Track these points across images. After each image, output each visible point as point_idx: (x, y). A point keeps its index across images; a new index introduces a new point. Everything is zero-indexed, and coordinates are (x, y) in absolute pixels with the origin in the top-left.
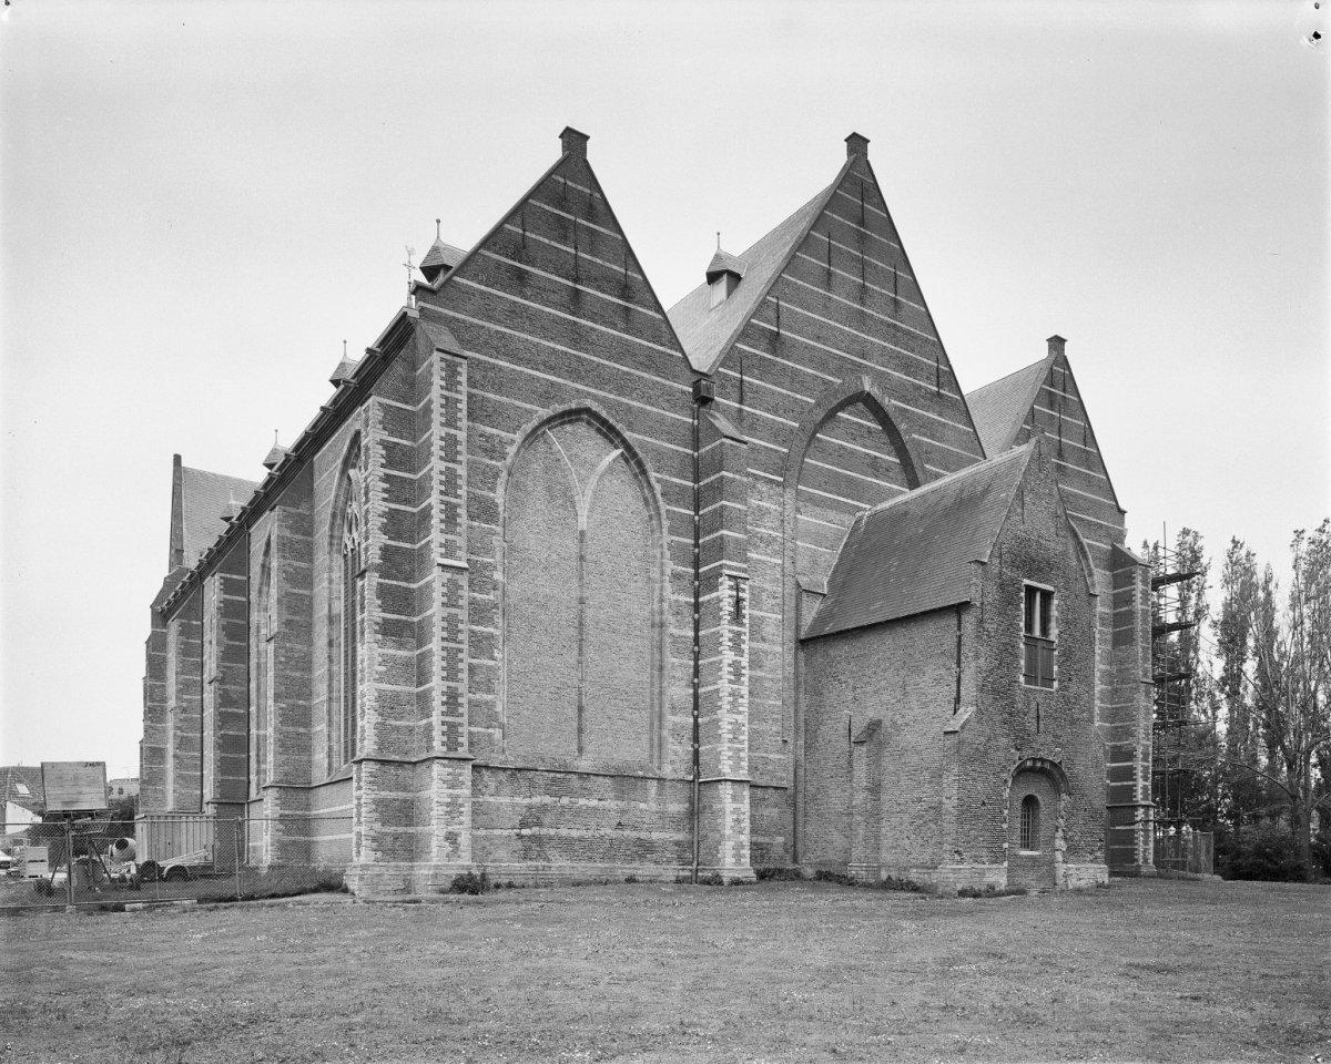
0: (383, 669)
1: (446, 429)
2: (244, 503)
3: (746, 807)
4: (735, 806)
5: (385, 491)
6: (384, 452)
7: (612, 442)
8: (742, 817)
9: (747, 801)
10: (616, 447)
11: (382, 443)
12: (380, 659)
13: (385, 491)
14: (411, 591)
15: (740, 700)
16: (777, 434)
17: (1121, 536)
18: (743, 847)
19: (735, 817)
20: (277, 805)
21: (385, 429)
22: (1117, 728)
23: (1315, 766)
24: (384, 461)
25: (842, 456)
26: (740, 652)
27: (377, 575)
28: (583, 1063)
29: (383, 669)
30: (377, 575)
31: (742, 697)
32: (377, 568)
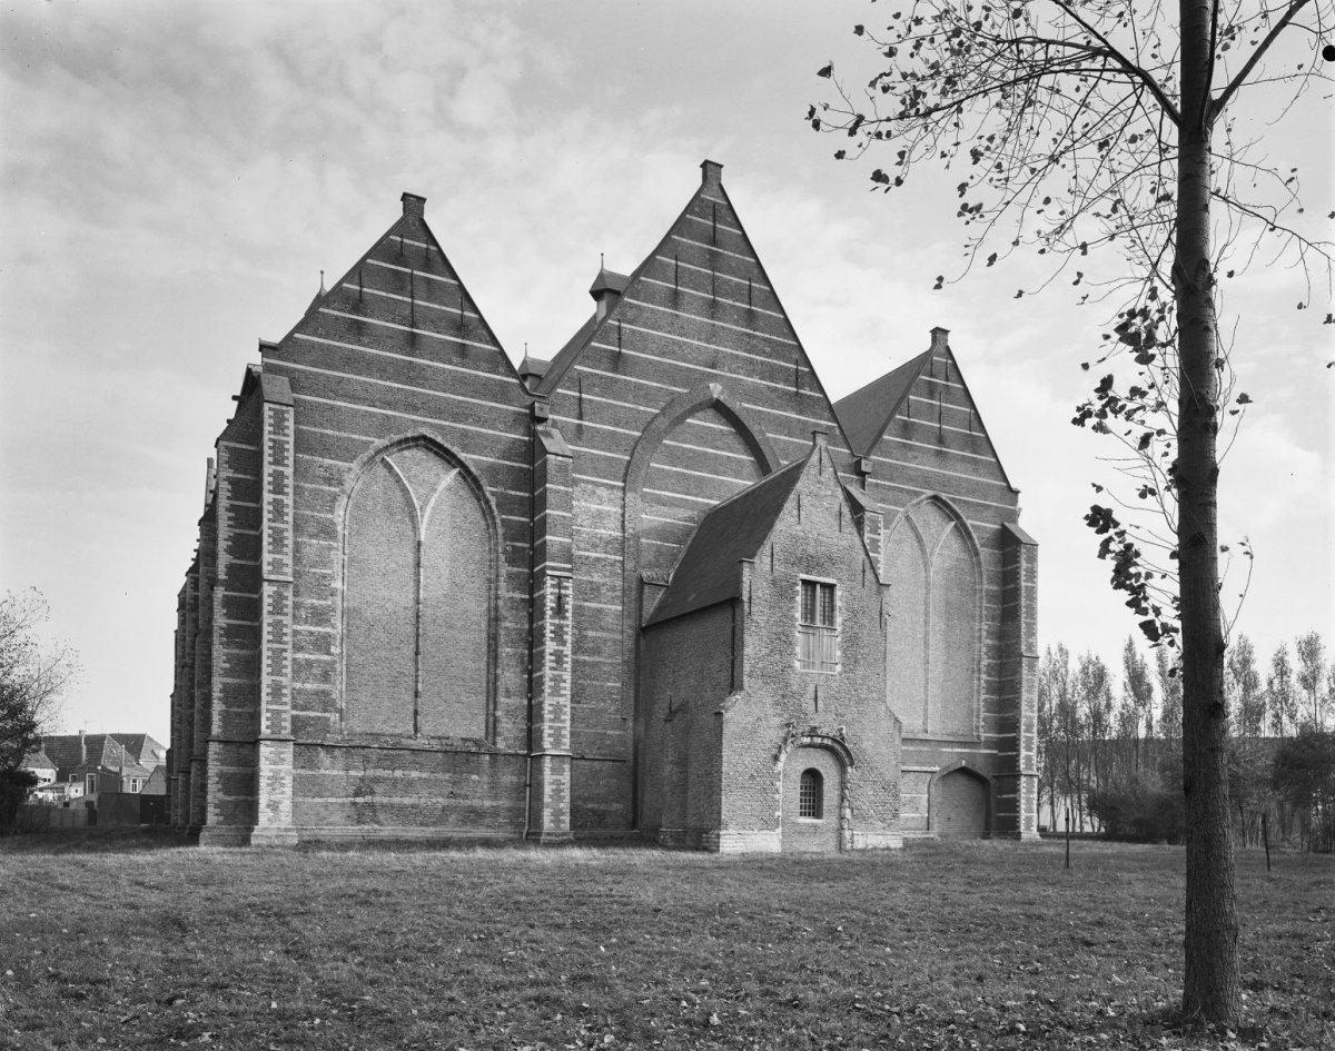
0: (228, 665)
5: (230, 518)
15: (562, 685)
16: (612, 441)
17: (1013, 516)
19: (554, 787)
27: (223, 589)
32: (224, 583)
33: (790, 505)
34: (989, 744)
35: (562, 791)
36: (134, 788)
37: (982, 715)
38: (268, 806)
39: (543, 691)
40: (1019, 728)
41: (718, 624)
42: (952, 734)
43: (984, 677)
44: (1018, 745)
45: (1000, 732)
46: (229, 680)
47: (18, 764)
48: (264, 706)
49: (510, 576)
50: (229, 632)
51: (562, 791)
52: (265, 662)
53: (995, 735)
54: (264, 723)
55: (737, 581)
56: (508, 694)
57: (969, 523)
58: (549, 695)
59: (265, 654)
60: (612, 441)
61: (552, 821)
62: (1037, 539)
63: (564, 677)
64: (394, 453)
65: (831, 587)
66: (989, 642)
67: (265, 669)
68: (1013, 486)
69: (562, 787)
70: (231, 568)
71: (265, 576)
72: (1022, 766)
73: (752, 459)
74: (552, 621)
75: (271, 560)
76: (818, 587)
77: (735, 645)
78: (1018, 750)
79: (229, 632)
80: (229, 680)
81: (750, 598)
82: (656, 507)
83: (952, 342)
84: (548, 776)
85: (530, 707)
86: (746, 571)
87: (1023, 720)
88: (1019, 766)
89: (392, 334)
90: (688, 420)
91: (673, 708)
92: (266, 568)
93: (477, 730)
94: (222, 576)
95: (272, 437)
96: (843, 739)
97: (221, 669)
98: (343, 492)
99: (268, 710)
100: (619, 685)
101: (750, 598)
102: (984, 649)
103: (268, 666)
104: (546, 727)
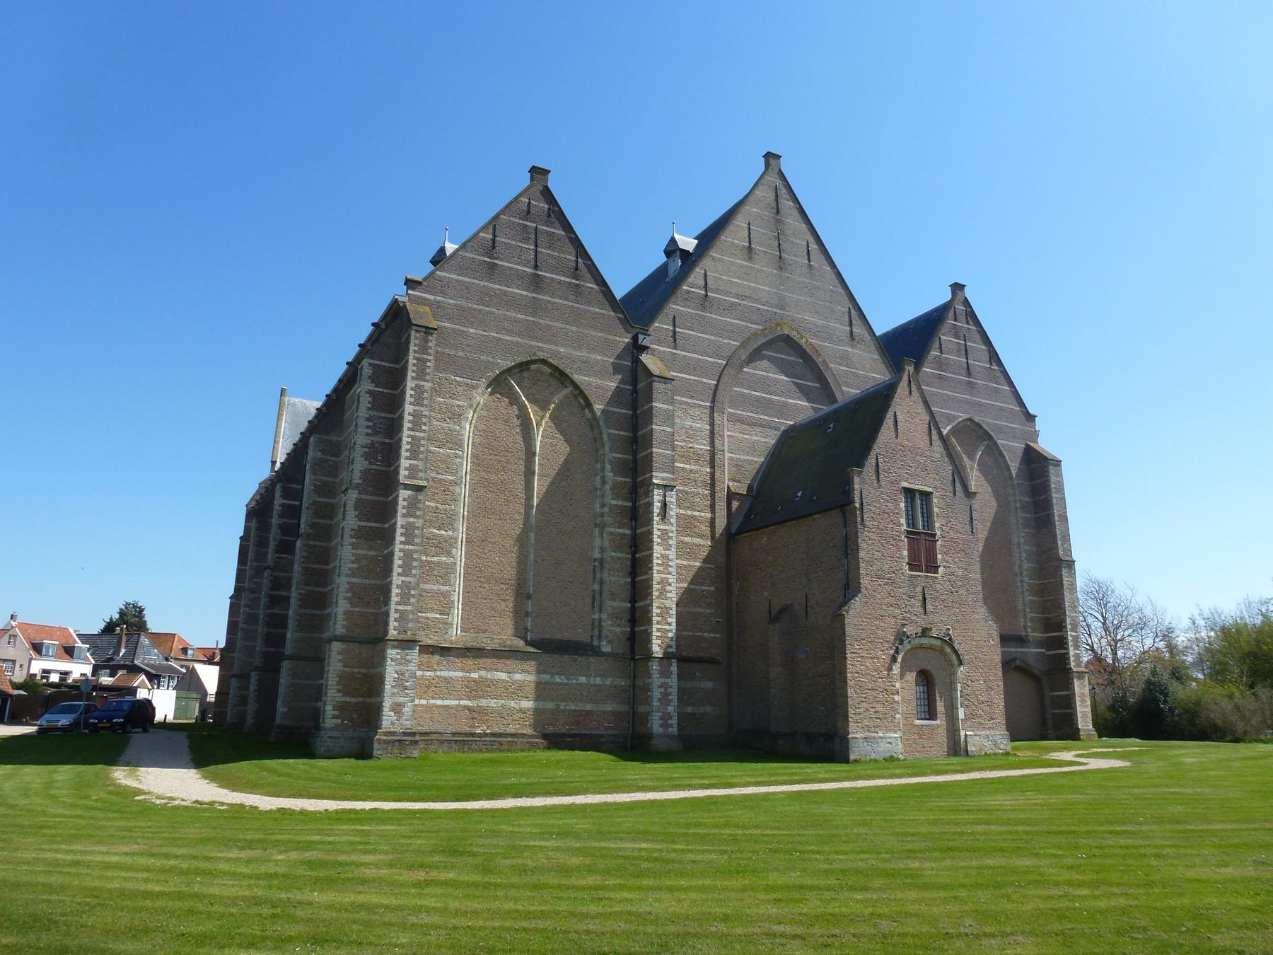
0: (355, 566)
1: (416, 382)
2: (319, 404)
3: (673, 681)
4: (662, 680)
5: (368, 427)
6: (370, 399)
7: (562, 383)
8: (670, 690)
9: (675, 676)
10: (566, 387)
11: (370, 393)
12: (353, 558)
13: (368, 427)
14: (331, 525)
15: (668, 588)
16: (705, 370)
17: (1035, 435)
18: (671, 718)
19: (662, 690)
20: (289, 675)
21: (372, 382)
22: (1046, 601)
23: (558, 706)
24: (369, 406)
25: (764, 384)
26: (668, 547)
27: (357, 492)
28: (709, 954)
29: (355, 566)
30: (357, 492)
31: (670, 585)
32: (357, 487)
33: (889, 421)
34: (1040, 644)
35: (670, 694)
36: (516, 691)
37: (1029, 616)
38: (393, 710)
39: (651, 594)
40: (1065, 627)
41: (824, 524)
42: (151, 666)
43: (1026, 579)
44: (1067, 643)
45: (1046, 631)
46: (354, 580)
47: (48, 680)
48: (393, 606)
49: (615, 486)
50: (360, 534)
51: (670, 694)
52: (397, 562)
53: (1040, 635)
54: (393, 624)
55: (849, 483)
56: (613, 597)
57: (999, 442)
58: (657, 598)
59: (398, 554)
60: (705, 370)
61: (661, 726)
62: (1059, 457)
63: (670, 581)
64: (516, 374)
65: (926, 496)
66: (1026, 547)
67: (397, 570)
68: (1031, 411)
69: (670, 690)
70: (365, 473)
71: (402, 479)
72: (1072, 664)
73: (818, 385)
74: (659, 527)
75: (408, 466)
76: (917, 495)
77: (849, 548)
78: (1067, 649)
79: (360, 534)
80: (354, 580)
81: (862, 504)
82: (739, 425)
83: (968, 293)
84: (656, 679)
85: (633, 610)
86: (856, 479)
87: (1068, 621)
88: (1069, 664)
89: (520, 275)
90: (763, 352)
91: (773, 614)
92: (403, 473)
93: (33, 662)
94: (357, 480)
95: (417, 355)
96: (950, 639)
97: (350, 569)
98: (471, 406)
99: (396, 611)
100: (712, 589)
101: (862, 504)
102: (1024, 555)
103: (399, 566)
104: (654, 630)
